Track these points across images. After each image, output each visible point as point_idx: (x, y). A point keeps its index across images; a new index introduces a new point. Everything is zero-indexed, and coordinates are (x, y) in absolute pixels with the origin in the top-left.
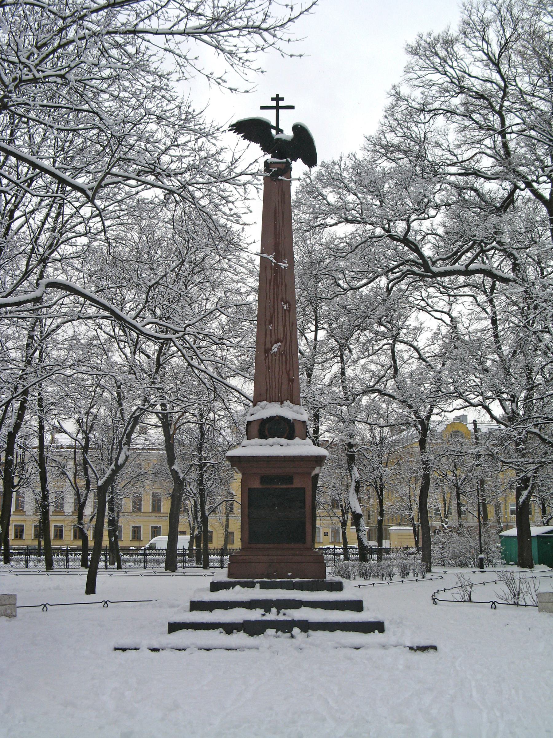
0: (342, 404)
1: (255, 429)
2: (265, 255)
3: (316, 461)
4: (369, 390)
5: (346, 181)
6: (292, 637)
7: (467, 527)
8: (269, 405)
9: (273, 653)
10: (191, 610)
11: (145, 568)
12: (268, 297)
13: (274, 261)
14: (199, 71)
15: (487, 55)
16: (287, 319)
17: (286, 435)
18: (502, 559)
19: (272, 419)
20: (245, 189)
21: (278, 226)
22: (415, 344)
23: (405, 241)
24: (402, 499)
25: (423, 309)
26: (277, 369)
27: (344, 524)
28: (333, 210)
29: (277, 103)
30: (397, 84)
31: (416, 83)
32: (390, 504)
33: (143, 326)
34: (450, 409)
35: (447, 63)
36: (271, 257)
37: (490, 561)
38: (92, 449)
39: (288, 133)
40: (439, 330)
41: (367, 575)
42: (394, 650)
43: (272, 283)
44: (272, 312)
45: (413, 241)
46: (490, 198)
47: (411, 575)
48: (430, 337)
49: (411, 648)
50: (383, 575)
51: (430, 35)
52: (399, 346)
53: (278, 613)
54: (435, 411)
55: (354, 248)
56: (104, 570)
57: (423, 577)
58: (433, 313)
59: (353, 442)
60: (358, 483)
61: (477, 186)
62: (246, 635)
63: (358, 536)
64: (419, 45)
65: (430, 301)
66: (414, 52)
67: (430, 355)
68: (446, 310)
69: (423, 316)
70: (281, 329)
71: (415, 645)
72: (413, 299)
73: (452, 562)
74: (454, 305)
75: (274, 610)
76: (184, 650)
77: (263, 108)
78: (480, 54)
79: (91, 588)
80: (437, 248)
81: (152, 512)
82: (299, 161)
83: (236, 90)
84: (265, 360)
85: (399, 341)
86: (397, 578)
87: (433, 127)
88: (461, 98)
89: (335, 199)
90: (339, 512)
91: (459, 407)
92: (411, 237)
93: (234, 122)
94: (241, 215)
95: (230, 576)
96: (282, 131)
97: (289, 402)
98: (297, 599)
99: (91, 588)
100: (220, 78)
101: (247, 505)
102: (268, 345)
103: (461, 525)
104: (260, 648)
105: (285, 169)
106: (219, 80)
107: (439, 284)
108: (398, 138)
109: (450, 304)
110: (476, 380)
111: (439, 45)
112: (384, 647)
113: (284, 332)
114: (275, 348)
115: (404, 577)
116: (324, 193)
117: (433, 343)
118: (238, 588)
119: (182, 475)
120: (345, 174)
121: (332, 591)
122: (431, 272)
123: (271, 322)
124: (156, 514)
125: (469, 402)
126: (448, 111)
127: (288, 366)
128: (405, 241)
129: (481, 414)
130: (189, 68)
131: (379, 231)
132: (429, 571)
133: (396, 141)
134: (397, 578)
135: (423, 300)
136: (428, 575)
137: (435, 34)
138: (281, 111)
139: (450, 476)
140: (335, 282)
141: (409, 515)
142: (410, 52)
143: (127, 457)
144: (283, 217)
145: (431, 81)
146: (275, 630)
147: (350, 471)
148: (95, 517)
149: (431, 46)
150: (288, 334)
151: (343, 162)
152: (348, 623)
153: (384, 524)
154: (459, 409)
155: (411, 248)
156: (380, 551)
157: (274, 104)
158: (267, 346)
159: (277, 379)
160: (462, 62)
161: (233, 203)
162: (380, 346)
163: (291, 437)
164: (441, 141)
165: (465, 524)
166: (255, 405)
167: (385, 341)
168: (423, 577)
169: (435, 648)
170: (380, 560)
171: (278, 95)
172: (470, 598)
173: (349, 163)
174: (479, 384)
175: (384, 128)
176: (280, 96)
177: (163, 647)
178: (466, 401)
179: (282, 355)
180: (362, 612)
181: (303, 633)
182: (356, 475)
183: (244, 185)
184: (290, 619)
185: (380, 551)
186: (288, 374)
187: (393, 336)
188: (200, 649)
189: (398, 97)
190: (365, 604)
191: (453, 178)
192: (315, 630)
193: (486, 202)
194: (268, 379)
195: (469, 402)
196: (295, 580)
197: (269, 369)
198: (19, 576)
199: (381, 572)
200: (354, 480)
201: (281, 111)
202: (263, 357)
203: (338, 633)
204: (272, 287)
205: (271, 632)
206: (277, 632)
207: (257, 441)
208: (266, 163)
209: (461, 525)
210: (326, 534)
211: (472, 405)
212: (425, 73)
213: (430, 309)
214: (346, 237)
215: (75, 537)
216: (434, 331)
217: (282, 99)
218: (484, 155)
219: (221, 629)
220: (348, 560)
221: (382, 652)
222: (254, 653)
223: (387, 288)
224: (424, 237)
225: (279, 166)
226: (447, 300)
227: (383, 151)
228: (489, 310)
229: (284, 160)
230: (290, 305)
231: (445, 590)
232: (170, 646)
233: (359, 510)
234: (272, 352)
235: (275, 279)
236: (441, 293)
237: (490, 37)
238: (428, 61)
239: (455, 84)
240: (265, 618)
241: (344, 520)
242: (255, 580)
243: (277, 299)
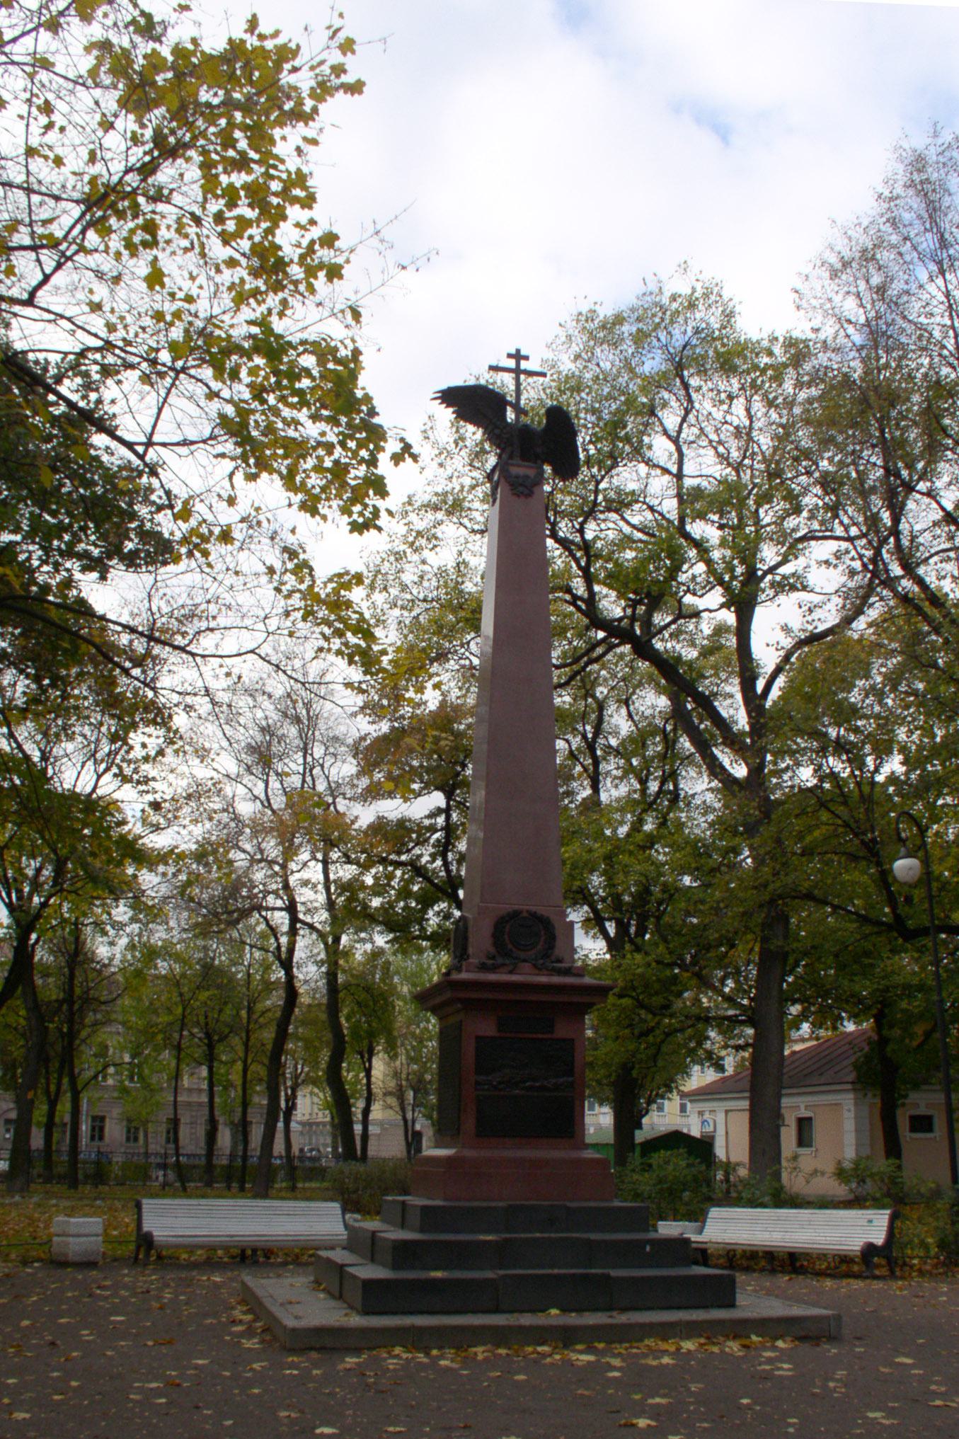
29: (518, 364)
157: (511, 363)
171: (518, 351)
217: (526, 358)
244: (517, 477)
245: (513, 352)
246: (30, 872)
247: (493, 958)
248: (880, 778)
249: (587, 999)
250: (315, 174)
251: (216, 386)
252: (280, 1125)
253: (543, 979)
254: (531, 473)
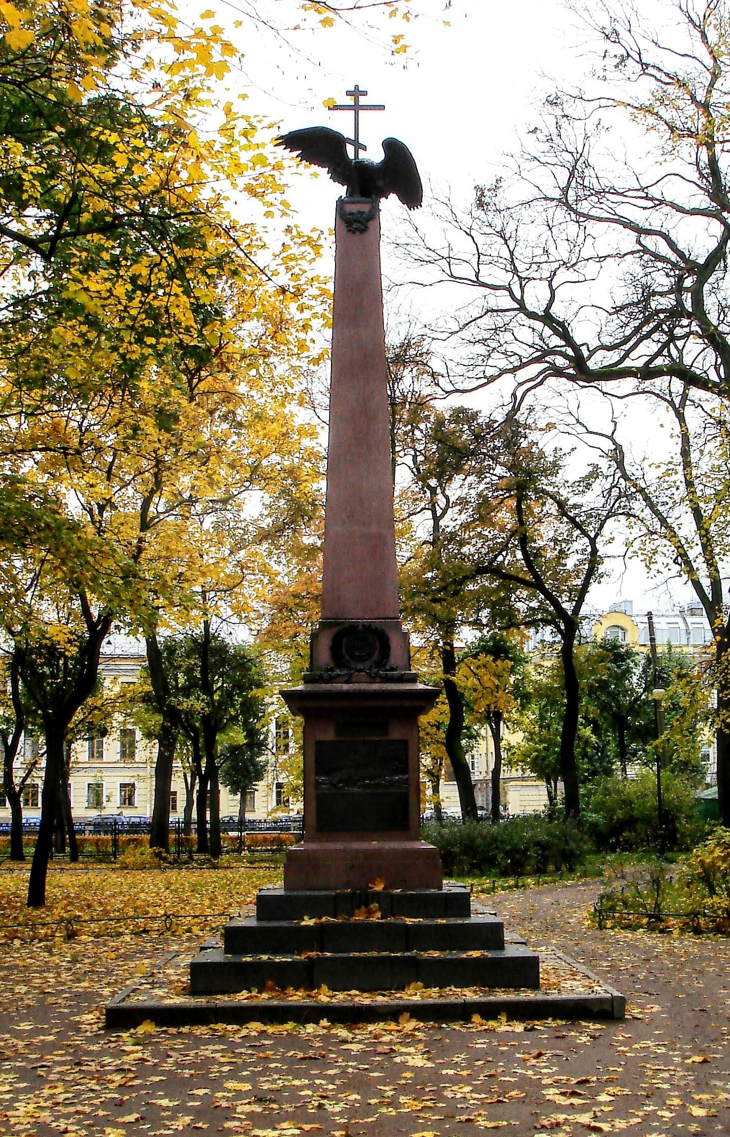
23: (547, 318)
29: (356, 101)
30: (487, 182)
39: (375, 155)
82: (393, 197)
92: (558, 311)
128: (547, 318)
157: (350, 101)
171: (357, 87)
217: (365, 93)
244: (352, 214)
247: (332, 670)
248: (118, 53)
249: (417, 703)
250: (543, 97)
253: (376, 687)
254: (366, 208)
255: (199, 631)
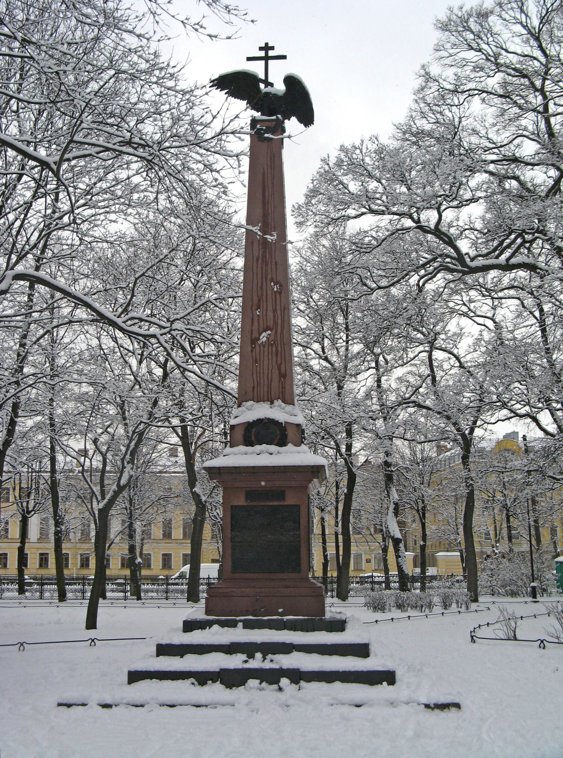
0: (374, 417)
1: (239, 434)
2: (250, 227)
3: (313, 472)
4: (404, 402)
5: (369, 168)
6: (280, 689)
7: (518, 553)
8: (256, 405)
9: (252, 711)
10: (158, 655)
11: (167, 599)
12: (255, 277)
13: (259, 233)
14: (173, 17)
15: (524, 27)
16: (278, 303)
17: (276, 442)
18: (558, 587)
19: (259, 422)
20: (239, 161)
21: (267, 194)
22: (455, 351)
23: (437, 232)
24: (449, 524)
25: (465, 315)
26: (266, 363)
27: (385, 550)
28: (355, 198)
29: (267, 53)
30: (426, 63)
31: (448, 61)
32: (434, 527)
33: (124, 322)
34: (493, 420)
35: (482, 39)
36: (256, 229)
37: (544, 590)
38: (110, 472)
39: (280, 87)
40: (481, 335)
41: (404, 606)
42: (404, 708)
43: (260, 261)
44: (260, 295)
45: (446, 232)
46: (533, 185)
47: (454, 605)
48: (471, 344)
49: (427, 706)
50: (422, 607)
51: (461, 8)
52: (438, 355)
53: (264, 659)
54: (479, 423)
55: (380, 241)
56: (123, 601)
57: (467, 608)
58: (476, 319)
59: (389, 460)
60: (396, 504)
61: (518, 173)
62: (222, 687)
63: (398, 563)
64: (450, 20)
65: (472, 306)
66: (444, 27)
67: (473, 364)
68: (490, 315)
69: (465, 321)
70: (270, 314)
71: (432, 702)
72: (453, 304)
73: (502, 591)
74: (498, 309)
75: (259, 655)
76: (142, 706)
77: (249, 59)
78: (519, 28)
79: (91, 623)
80: (474, 244)
81: (183, 539)
82: (294, 119)
83: (216, 37)
84: (252, 351)
85: (437, 349)
86: (438, 609)
87: (469, 111)
88: (499, 76)
89: (356, 187)
90: (379, 537)
91: (503, 418)
93: (216, 76)
94: (227, 185)
95: (207, 612)
96: (272, 85)
97: (280, 401)
98: (288, 642)
99: (91, 623)
100: (198, 24)
101: (229, 526)
102: (255, 334)
103: (511, 550)
104: (236, 705)
105: (275, 127)
106: (196, 27)
107: (481, 286)
108: (430, 125)
109: (494, 308)
110: (520, 387)
111: (471, 20)
112: (392, 704)
113: (274, 317)
114: (263, 338)
115: (445, 609)
116: (345, 181)
117: (475, 350)
118: (216, 627)
119: (204, 498)
120: (367, 160)
121: (331, 632)
122: (468, 267)
123: (259, 307)
124: (167, 541)
125: (514, 413)
126: (484, 92)
127: (279, 359)
129: (531, 428)
130: (164, 16)
131: (408, 223)
132: (476, 600)
133: (428, 127)
134: (438, 609)
135: (464, 304)
136: (474, 606)
137: (467, 8)
138: (270, 62)
139: (499, 496)
140: (362, 281)
141: (456, 540)
142: (441, 28)
143: (131, 476)
144: (273, 183)
145: (464, 59)
146: (259, 681)
147: (388, 492)
148: (107, 545)
149: (464, 22)
150: (279, 321)
151: (364, 146)
152: (349, 672)
153: (428, 551)
154: (503, 421)
155: (445, 242)
156: (423, 579)
158: (254, 335)
159: (266, 372)
160: (499, 38)
161: (218, 172)
162: (416, 353)
163: (282, 443)
164: (479, 128)
165: (516, 549)
166: (239, 406)
167: (421, 348)
168: (467, 608)
169: (457, 706)
170: (423, 589)
171: (267, 44)
172: (515, 635)
173: (373, 147)
174: (525, 392)
175: (414, 114)
176: (270, 45)
177: (116, 703)
178: (512, 411)
179: (272, 345)
180: (368, 659)
181: (293, 685)
182: (395, 496)
183: (237, 156)
184: (277, 667)
185: (423, 579)
186: (279, 369)
187: (429, 342)
188: (162, 705)
189: (428, 77)
190: (372, 648)
191: (492, 167)
192: (308, 681)
193: (528, 190)
194: (255, 375)
195: (514, 413)
196: (286, 618)
197: (256, 362)
198: (27, 608)
199: (420, 603)
200: (392, 501)
201: (270, 62)
202: (249, 349)
203: (338, 685)
204: (260, 266)
205: (253, 683)
206: (260, 684)
207: (242, 448)
208: (254, 122)
209: (511, 550)
210: (368, 561)
211: (517, 415)
212: (458, 50)
213: (472, 314)
214: (371, 230)
215: (123, 565)
216: (475, 337)
217: (272, 48)
218: (525, 139)
219: (192, 680)
220: (390, 589)
221: (390, 710)
222: (228, 711)
223: (418, 285)
224: (461, 233)
225: (269, 124)
226: (491, 304)
227: (414, 139)
228: (537, 314)
229: (274, 117)
230: (281, 286)
231: (488, 624)
232: (125, 701)
233: (398, 535)
234: (259, 342)
235: (264, 256)
236: (484, 296)
237: (529, 9)
238: (460, 38)
239: (492, 61)
240: (247, 666)
241: (385, 545)
242: (238, 618)
243: (266, 281)
245: (264, 45)
246: (376, 407)
251: (373, 532)
252: (341, 553)
255: (479, 220)
